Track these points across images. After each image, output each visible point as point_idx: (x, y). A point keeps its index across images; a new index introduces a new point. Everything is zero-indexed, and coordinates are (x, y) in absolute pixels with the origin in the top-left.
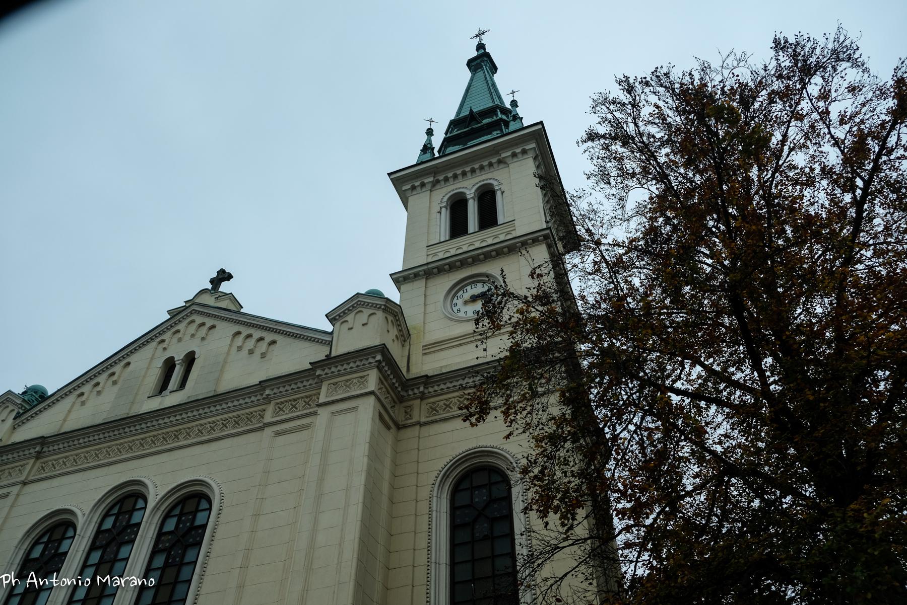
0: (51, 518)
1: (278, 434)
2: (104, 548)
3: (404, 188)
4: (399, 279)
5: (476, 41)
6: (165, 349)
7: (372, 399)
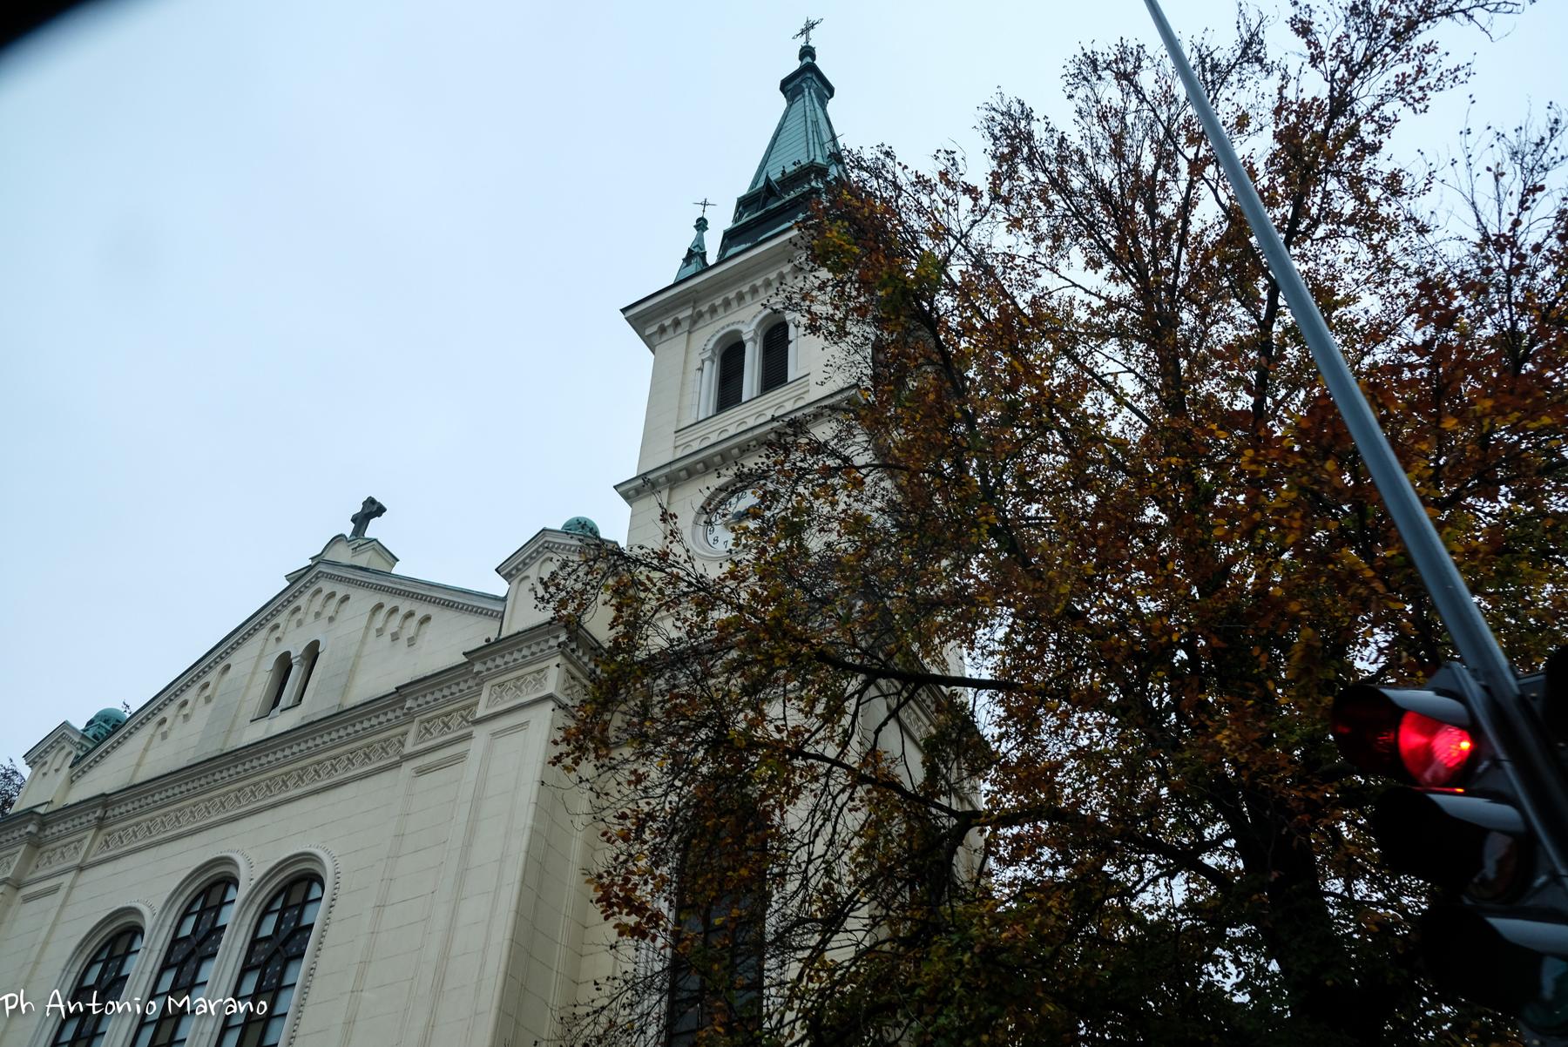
0: (112, 922)
1: (421, 772)
2: (180, 966)
3: (648, 332)
4: (633, 491)
5: (801, 41)
6: (278, 639)
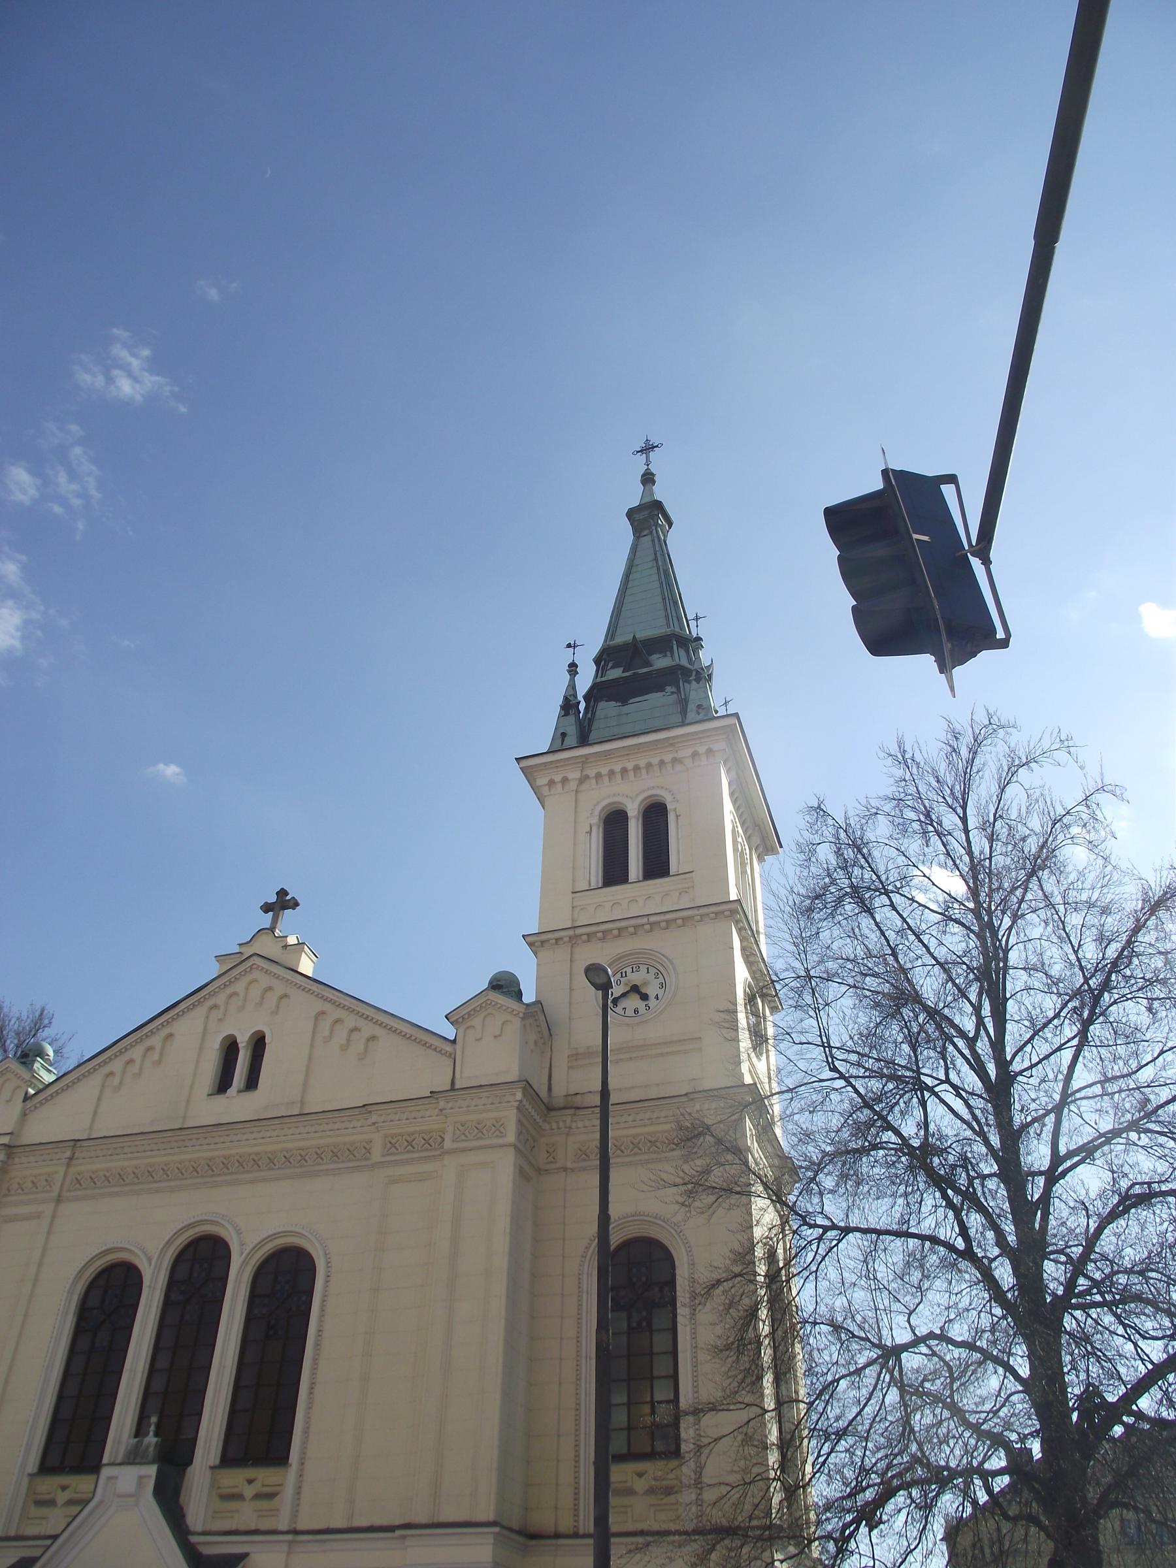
7: (512, 1150)
